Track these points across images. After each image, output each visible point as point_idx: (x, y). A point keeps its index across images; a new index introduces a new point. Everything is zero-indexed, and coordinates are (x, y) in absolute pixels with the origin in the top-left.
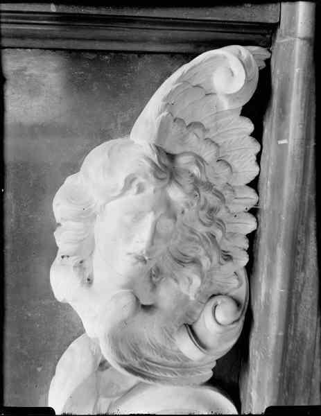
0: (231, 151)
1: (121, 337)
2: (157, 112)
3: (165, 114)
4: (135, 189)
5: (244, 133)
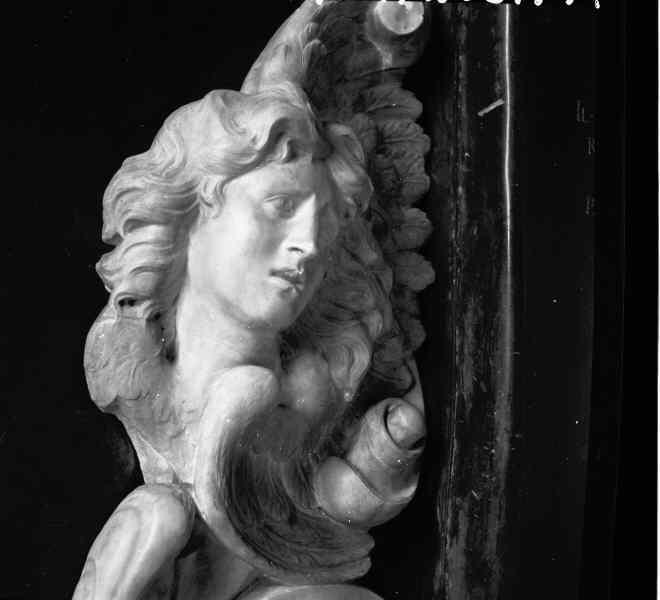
0: (391, 143)
1: (239, 472)
2: (306, 36)
3: (316, 41)
4: (284, 151)
5: (408, 115)
